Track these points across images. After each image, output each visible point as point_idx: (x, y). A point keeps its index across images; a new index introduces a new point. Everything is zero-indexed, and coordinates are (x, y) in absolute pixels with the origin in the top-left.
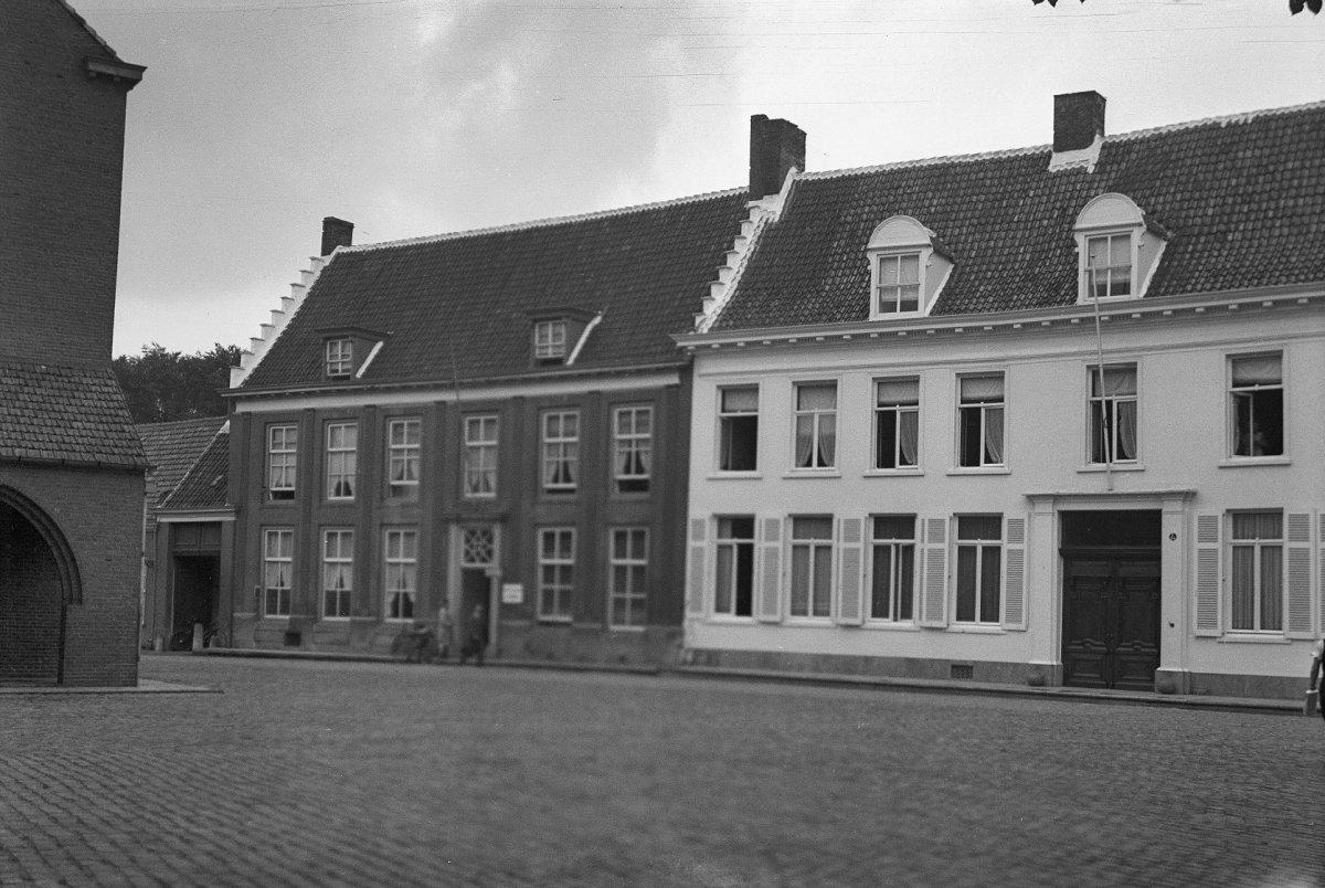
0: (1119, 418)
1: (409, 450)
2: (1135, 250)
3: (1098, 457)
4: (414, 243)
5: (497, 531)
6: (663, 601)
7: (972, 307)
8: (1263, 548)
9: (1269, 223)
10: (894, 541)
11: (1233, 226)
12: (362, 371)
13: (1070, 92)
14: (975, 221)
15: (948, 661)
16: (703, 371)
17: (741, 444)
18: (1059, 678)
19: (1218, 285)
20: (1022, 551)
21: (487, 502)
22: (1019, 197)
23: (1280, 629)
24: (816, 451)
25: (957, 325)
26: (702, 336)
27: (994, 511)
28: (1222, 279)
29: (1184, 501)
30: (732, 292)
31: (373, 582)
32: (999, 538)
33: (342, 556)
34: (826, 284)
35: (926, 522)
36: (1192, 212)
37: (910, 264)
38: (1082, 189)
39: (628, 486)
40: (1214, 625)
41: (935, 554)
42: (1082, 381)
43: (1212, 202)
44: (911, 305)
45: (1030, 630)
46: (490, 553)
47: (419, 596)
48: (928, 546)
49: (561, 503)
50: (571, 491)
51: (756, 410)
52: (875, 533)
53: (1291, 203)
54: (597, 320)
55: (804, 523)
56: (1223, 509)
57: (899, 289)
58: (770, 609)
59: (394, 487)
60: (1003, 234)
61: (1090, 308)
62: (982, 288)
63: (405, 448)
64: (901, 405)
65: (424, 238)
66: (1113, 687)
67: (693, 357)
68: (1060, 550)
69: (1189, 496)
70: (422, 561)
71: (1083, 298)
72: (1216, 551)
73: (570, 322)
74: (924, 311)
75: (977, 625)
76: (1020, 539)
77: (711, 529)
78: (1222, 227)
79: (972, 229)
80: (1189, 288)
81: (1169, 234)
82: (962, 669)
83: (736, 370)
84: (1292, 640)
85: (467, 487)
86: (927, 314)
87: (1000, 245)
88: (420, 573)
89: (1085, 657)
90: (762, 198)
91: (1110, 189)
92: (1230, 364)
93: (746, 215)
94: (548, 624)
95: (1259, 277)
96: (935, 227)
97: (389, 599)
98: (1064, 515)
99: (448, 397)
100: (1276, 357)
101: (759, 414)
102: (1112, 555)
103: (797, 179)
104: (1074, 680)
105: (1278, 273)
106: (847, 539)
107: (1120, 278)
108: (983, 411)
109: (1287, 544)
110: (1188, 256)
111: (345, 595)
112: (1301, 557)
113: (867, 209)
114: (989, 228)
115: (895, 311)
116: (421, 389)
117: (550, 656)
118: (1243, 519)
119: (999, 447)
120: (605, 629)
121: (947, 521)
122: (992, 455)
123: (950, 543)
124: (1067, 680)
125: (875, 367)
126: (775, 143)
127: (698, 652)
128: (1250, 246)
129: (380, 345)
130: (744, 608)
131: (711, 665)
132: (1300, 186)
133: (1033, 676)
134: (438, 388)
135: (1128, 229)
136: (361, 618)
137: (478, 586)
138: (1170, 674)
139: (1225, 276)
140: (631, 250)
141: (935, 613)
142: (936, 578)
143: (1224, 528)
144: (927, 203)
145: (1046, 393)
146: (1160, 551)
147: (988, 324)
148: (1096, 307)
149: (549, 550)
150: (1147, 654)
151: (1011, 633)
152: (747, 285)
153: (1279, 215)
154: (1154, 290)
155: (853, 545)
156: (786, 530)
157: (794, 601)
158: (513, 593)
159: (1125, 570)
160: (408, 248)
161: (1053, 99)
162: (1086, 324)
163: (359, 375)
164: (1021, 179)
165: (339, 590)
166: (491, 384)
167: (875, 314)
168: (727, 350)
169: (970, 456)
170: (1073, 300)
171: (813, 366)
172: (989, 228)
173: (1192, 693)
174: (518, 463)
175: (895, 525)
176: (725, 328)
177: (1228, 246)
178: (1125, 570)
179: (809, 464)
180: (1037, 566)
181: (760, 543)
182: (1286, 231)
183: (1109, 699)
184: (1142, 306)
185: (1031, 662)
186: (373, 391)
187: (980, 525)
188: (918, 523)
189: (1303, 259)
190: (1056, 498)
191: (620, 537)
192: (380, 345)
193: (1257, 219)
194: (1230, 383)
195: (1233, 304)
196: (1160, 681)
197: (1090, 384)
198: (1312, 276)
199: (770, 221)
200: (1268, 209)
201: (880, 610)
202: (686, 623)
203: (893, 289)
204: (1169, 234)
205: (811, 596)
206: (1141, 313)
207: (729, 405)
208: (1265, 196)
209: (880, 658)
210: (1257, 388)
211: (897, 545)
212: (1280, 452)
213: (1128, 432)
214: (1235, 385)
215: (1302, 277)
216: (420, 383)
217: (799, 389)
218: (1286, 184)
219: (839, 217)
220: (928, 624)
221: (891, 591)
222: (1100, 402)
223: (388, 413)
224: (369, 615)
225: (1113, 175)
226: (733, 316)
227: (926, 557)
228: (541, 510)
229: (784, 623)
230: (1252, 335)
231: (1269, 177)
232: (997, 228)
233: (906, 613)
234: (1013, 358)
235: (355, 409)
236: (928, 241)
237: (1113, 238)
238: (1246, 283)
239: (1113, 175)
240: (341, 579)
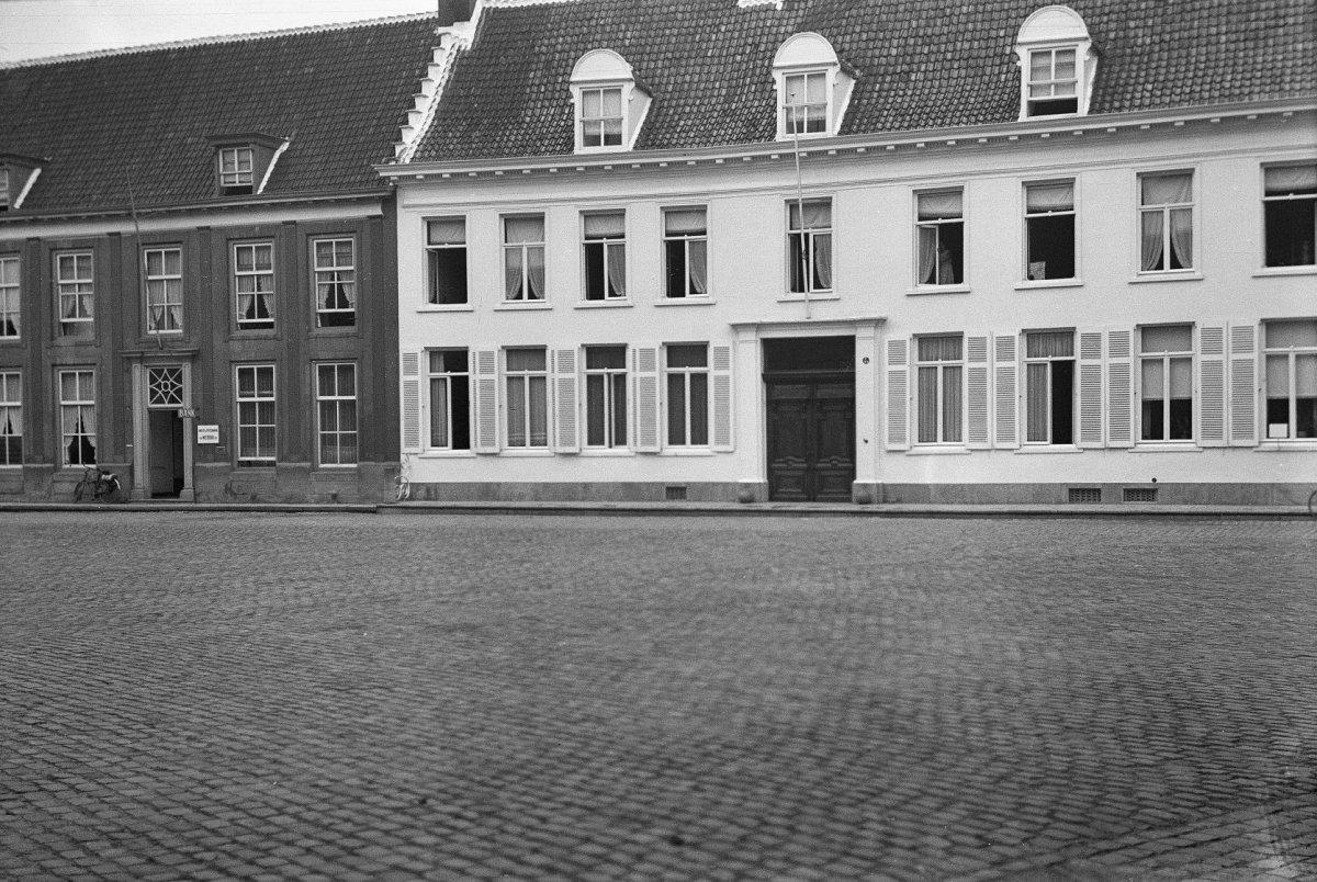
0: (814, 251)
1: (80, 285)
2: (625, 105)
3: (798, 285)
4: (64, 60)
5: (186, 369)
6: (377, 438)
7: (674, 141)
8: (531, 379)
9: (948, 65)
10: (606, 370)
11: (915, 67)
12: (20, 201)
14: (670, 55)
15: (663, 484)
16: (406, 202)
17: (450, 278)
18: (765, 495)
19: (906, 124)
21: (174, 339)
22: (711, 32)
23: (960, 440)
24: (526, 285)
25: (889, 143)
26: (405, 167)
27: (957, 330)
28: (911, 118)
30: (429, 121)
31: (47, 427)
32: (544, 369)
33: (8, 400)
34: (526, 115)
35: (477, 354)
36: (877, 52)
37: (613, 98)
38: (772, 25)
39: (331, 320)
40: (1012, 439)
41: (646, 382)
42: (782, 214)
43: (895, 42)
44: (613, 139)
45: (738, 451)
46: (179, 392)
47: (100, 439)
49: (258, 338)
50: (270, 325)
51: (464, 243)
52: (668, 361)
53: (967, 45)
54: (285, 147)
55: (515, 354)
56: (1018, 330)
57: (603, 123)
58: (488, 441)
59: (65, 325)
60: (698, 69)
61: (791, 144)
62: (682, 123)
63: (76, 287)
64: (608, 238)
65: (74, 55)
66: (814, 500)
67: (396, 187)
68: (763, 375)
69: (879, 323)
70: (101, 403)
71: (781, 135)
72: (903, 372)
73: (257, 149)
74: (628, 144)
75: (688, 449)
76: (726, 367)
77: (423, 362)
78: (905, 67)
79: (667, 63)
80: (879, 126)
81: (857, 72)
82: (676, 491)
83: (443, 201)
84: (972, 450)
85: (150, 322)
86: (630, 148)
87: (696, 79)
88: (100, 416)
89: (789, 473)
90: (452, 24)
91: (802, 28)
93: (437, 41)
94: (249, 464)
95: (942, 118)
96: (631, 59)
97: (66, 445)
98: (766, 343)
99: (126, 228)
100: (957, 192)
101: (1076, 211)
102: (811, 383)
103: (487, 6)
104: (780, 495)
105: (958, 114)
106: (483, 371)
107: (816, 115)
108: (687, 244)
109: (967, 364)
110: (875, 95)
111: (15, 442)
112: (979, 376)
113: (561, 40)
114: (684, 63)
115: (599, 145)
116: (91, 220)
117: (254, 499)
118: (928, 343)
119: (703, 279)
120: (314, 468)
122: (696, 285)
123: (660, 372)
124: (773, 496)
125: (509, 202)
127: (415, 486)
128: (932, 86)
129: (37, 172)
130: (462, 441)
131: (430, 500)
132: (975, 30)
133: (744, 494)
134: (111, 218)
135: (1073, 43)
136: (37, 466)
137: (168, 428)
138: (865, 486)
139: (911, 115)
140: (314, 73)
141: (649, 438)
142: (648, 405)
143: (912, 350)
144: (621, 35)
145: (746, 225)
146: (854, 374)
148: (796, 144)
149: (246, 386)
150: (845, 469)
151: (720, 455)
152: (444, 114)
153: (957, 57)
154: (846, 129)
155: (649, 374)
156: (500, 361)
157: (511, 431)
158: (209, 434)
159: (824, 392)
160: (57, 65)
162: (787, 159)
163: (17, 206)
164: (711, 13)
165: (7, 435)
166: (172, 215)
167: (580, 148)
168: (432, 181)
169: (675, 287)
170: (772, 137)
171: (521, 198)
172: (684, 63)
173: (885, 502)
174: (207, 300)
175: (606, 355)
176: (427, 159)
177: (911, 85)
178: (824, 392)
181: (475, 376)
182: (963, 72)
183: (818, 512)
184: (1087, 123)
185: (741, 481)
186: (35, 222)
187: (687, 353)
188: (548, 353)
189: (980, 99)
190: (759, 327)
191: (326, 373)
192: (37, 172)
193: (937, 60)
194: (1263, 193)
195: (920, 142)
196: (856, 493)
197: (788, 218)
198: (989, 117)
199: (463, 48)
200: (946, 51)
201: (595, 438)
202: (403, 457)
203: (597, 123)
204: (857, 72)
205: (528, 427)
206: (1151, 125)
207: (433, 239)
208: (944, 39)
209: (597, 484)
210: (940, 221)
211: (609, 374)
212: (1071, 274)
213: (823, 262)
214: (921, 219)
215: (998, 116)
216: (89, 214)
217: (429, 224)
218: (961, 27)
219: (533, 47)
220: (644, 449)
221: (606, 420)
222: (799, 235)
223: (54, 246)
224: (44, 461)
225: (801, 13)
226: (433, 147)
228: (236, 346)
229: (582, 454)
230: (937, 172)
231: (946, 20)
232: (692, 62)
233: (621, 439)
234: (713, 193)
235: (350, 221)
236: (1086, 34)
237: (604, 91)
238: (931, 122)
239: (801, 13)
240: (10, 425)
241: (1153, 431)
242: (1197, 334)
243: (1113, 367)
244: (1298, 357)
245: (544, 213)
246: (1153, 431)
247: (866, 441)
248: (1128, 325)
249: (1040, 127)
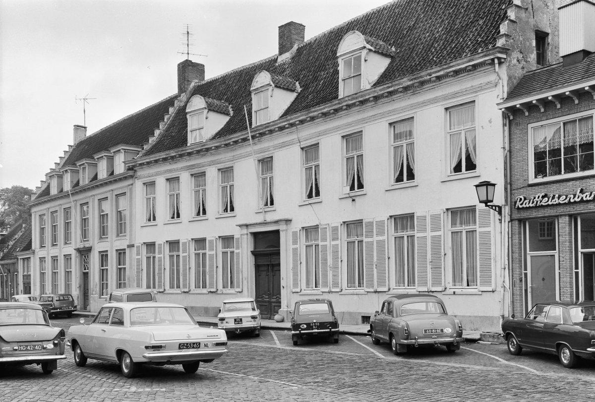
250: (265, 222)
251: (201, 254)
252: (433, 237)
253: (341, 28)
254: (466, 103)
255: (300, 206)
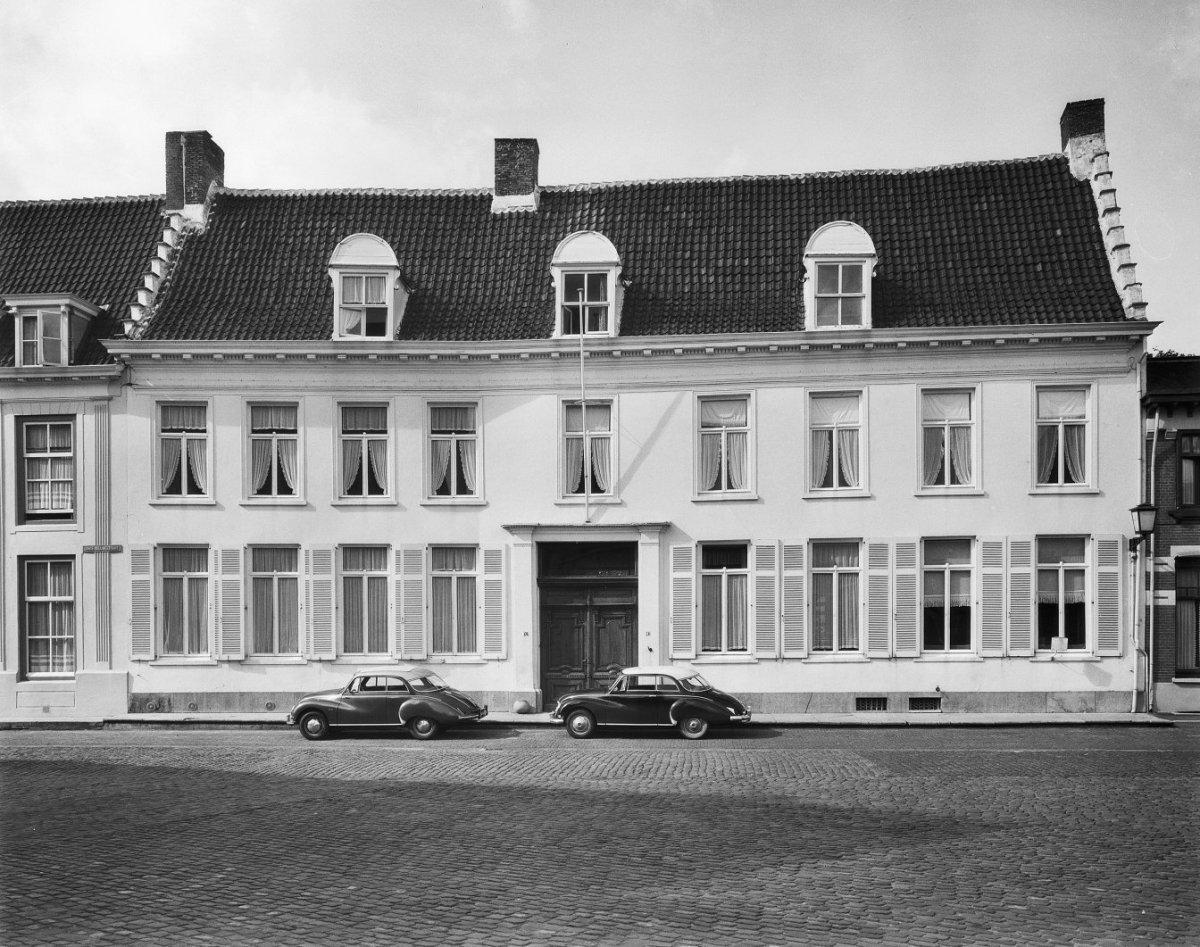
13: (512, 137)
20: (499, 582)
27: (203, 543)
29: (660, 533)
48: (311, 577)
69: (664, 528)
76: (497, 570)
92: (160, 410)
102: (585, 581)
121: (694, 549)
126: (196, 156)
135: (384, 271)
147: (1034, 337)
161: (493, 143)
171: (277, 384)
175: (182, 556)
179: (1053, 479)
180: (514, 595)
188: (211, 554)
190: (536, 529)
206: (907, 343)
221: (946, 626)
226: (160, 327)
227: (402, 588)
241: (933, 640)
242: (480, 557)
243: (900, 578)
244: (953, 572)
245: (298, 403)
246: (933, 640)
247: (651, 650)
248: (914, 536)
249: (832, 338)
250: (588, 524)
251: (947, 574)
252: (900, 578)
253: (565, 232)
254: (961, 389)
255: (556, 504)
